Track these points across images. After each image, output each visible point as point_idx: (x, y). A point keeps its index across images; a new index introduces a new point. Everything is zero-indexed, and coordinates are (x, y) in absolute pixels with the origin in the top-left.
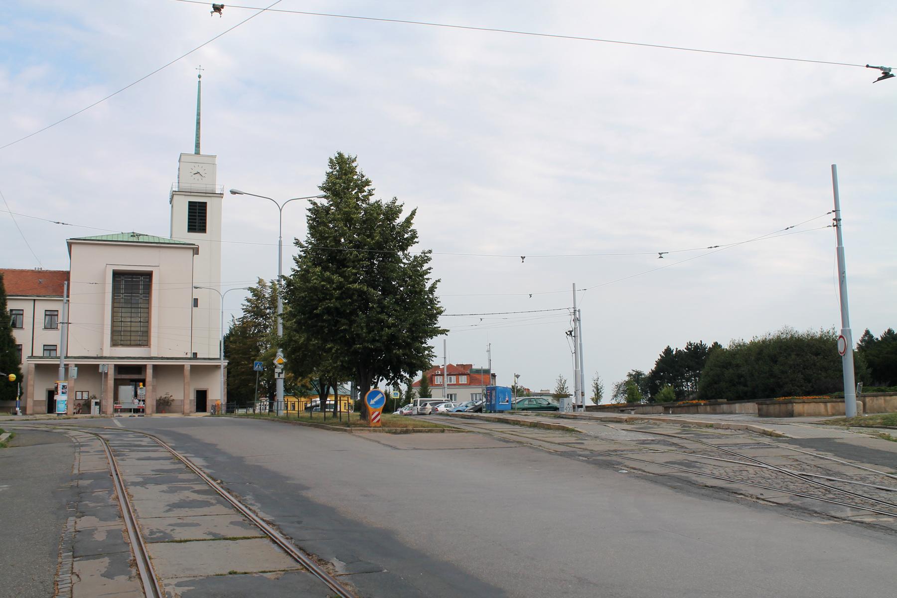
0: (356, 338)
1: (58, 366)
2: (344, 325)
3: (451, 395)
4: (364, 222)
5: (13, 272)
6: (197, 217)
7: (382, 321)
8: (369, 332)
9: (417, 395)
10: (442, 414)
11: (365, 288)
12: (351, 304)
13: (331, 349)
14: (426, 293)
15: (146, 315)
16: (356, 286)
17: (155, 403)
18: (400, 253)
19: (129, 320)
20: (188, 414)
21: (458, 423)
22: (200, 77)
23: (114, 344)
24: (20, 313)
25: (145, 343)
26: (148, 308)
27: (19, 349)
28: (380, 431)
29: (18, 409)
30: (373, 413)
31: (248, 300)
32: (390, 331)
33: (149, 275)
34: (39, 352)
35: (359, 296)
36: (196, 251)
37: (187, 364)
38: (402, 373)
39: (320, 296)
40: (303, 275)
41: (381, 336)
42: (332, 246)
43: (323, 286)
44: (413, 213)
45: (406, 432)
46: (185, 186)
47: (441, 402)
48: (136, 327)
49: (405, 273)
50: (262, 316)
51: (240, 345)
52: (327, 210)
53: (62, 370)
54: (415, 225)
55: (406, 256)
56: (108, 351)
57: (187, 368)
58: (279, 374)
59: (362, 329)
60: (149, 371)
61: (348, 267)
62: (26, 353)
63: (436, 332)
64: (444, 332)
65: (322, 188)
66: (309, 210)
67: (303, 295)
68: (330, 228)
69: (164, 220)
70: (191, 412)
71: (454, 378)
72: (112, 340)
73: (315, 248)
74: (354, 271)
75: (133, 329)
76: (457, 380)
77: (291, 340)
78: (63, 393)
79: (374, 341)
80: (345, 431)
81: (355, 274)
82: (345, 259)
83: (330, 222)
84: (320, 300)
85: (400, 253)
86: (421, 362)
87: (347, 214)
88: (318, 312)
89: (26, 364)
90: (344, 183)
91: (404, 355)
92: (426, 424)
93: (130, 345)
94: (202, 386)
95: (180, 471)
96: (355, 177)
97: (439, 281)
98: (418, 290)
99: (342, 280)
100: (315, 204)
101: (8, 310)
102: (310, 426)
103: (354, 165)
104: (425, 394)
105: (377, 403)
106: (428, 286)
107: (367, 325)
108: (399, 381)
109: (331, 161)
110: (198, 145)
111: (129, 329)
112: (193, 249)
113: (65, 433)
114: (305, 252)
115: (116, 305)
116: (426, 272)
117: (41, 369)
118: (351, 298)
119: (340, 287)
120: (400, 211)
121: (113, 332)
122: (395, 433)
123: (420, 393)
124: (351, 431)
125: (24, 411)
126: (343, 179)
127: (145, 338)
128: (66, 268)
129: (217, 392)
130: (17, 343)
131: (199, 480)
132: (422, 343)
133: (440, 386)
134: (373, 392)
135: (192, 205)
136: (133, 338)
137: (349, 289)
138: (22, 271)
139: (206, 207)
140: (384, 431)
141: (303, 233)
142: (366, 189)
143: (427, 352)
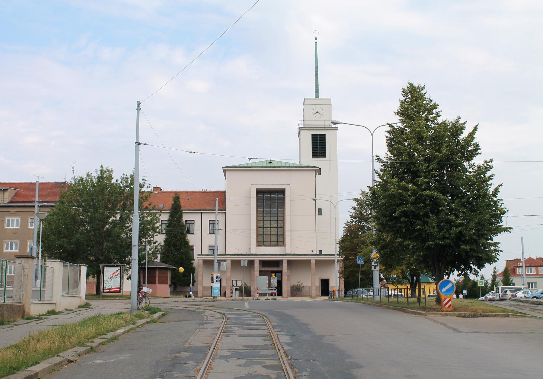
0: (430, 236)
1: (334, 260)
2: (418, 225)
3: (532, 284)
4: (433, 139)
5: (187, 193)
6: (319, 146)
7: (452, 221)
8: (440, 231)
9: (501, 283)
10: (520, 300)
11: (436, 194)
12: (424, 207)
13: (408, 245)
14: (490, 197)
15: (281, 222)
16: (427, 192)
17: (290, 289)
18: (466, 164)
19: (269, 226)
20: (315, 298)
21: (526, 309)
22: (316, 39)
23: (259, 244)
24: (192, 222)
25: (281, 243)
26: (283, 217)
27: (192, 248)
28: (451, 315)
29: (191, 293)
30: (445, 299)
31: (354, 208)
32: (458, 230)
33: (282, 192)
34: (206, 251)
35: (430, 200)
36: (318, 171)
37: (313, 259)
38: (471, 265)
39: (398, 202)
40: (384, 186)
41: (450, 234)
42: (406, 160)
43: (400, 193)
44: (475, 129)
45: (474, 316)
46: (309, 123)
47: (520, 290)
48: (274, 231)
49: (469, 179)
50: (365, 221)
51: (351, 243)
52: (402, 131)
53: (216, 264)
54: (478, 138)
55: (471, 166)
56: (255, 249)
57: (313, 262)
58: (375, 266)
59: (434, 228)
60: (285, 265)
61: (421, 177)
62: (197, 251)
63: (499, 230)
64: (506, 229)
65: (398, 113)
66: (388, 132)
67: (383, 201)
68: (405, 146)
69: (294, 149)
70: (317, 296)
71: (534, 270)
72: (257, 241)
73: (393, 162)
74: (425, 180)
75: (272, 233)
76: (537, 271)
77: (380, 239)
78: (217, 281)
79: (444, 238)
80: (421, 314)
81: (428, 183)
82: (418, 171)
83: (406, 141)
84: (398, 206)
85: (466, 164)
86: (488, 255)
87: (419, 133)
88: (396, 215)
89: (197, 261)
90: (415, 107)
91: (471, 250)
92: (495, 309)
93: (270, 245)
94: (325, 277)
95: (265, 347)
96: (424, 102)
97: (501, 185)
98: (482, 194)
99: (415, 188)
100: (392, 127)
101: (184, 220)
102: (395, 309)
103: (423, 92)
104: (507, 282)
105: (448, 291)
106: (491, 190)
107: (438, 226)
108: (468, 272)
109: (404, 91)
110: (317, 91)
111: (269, 233)
112: (315, 170)
113: (203, 312)
114: (385, 166)
115: (259, 215)
116: (489, 179)
117: (208, 264)
118: (424, 203)
119: (414, 193)
120: (464, 128)
121: (258, 236)
122: (464, 317)
123: (503, 282)
124: (425, 315)
125: (196, 294)
126: (415, 105)
127: (281, 240)
128: (223, 189)
129: (336, 283)
130: (191, 245)
131: (275, 357)
132: (488, 239)
133: (521, 276)
134: (446, 281)
135: (314, 137)
136: (272, 240)
137: (422, 195)
138: (193, 192)
139: (325, 138)
140: (454, 315)
141: (383, 151)
142: (434, 111)
143: (492, 248)
